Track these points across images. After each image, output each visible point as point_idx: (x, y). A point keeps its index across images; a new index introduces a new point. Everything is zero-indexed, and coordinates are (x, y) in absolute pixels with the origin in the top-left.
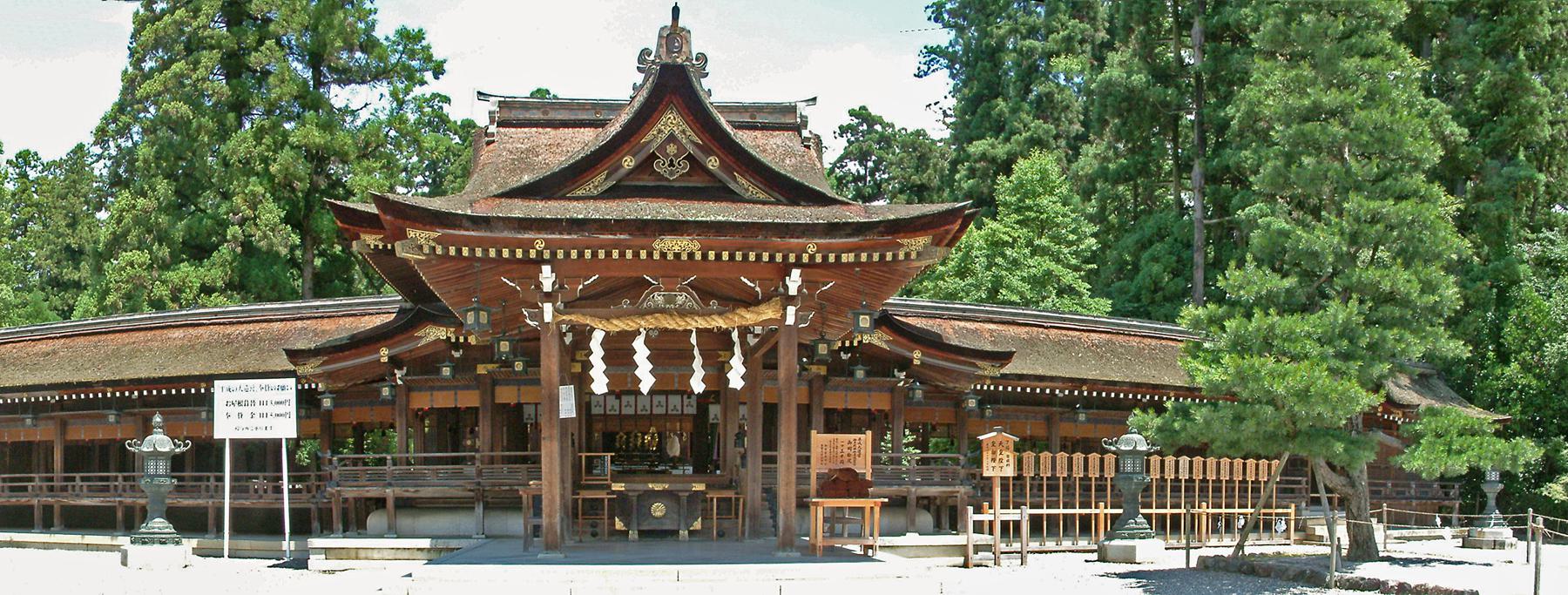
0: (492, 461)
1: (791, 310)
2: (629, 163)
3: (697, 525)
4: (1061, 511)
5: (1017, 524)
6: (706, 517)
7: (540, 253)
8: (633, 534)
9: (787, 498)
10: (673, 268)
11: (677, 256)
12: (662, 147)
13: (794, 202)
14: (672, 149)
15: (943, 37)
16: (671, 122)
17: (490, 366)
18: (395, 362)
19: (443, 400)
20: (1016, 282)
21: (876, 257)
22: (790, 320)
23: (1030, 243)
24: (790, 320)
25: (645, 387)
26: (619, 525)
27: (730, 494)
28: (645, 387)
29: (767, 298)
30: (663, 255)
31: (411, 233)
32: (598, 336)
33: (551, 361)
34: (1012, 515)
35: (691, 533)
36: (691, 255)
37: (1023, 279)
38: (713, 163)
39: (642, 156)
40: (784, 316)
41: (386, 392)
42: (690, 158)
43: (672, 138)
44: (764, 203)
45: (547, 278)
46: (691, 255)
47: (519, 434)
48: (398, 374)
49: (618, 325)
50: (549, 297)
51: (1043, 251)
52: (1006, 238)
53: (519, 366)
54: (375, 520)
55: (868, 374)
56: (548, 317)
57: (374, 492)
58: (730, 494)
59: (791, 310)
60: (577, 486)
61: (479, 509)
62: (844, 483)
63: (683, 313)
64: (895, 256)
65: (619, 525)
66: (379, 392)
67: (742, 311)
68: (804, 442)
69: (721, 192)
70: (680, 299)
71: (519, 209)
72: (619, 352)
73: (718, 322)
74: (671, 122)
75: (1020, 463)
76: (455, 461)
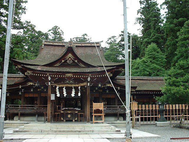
0: (40, 107)
1: (89, 83)
2: (63, 61)
3: (76, 119)
4: (154, 116)
5: (138, 119)
6: (78, 117)
7: (48, 76)
8: (64, 121)
9: (88, 114)
10: (69, 78)
11: (69, 76)
12: (68, 59)
13: (89, 67)
14: (70, 59)
15: (139, 16)
16: (70, 55)
17: (40, 90)
18: (22, 88)
19: (31, 95)
20: (148, 70)
21: (101, 76)
22: (89, 85)
23: (151, 61)
24: (89, 85)
25: (65, 96)
26: (62, 119)
27: (82, 113)
28: (65, 96)
29: (85, 82)
30: (67, 76)
31: (28, 71)
32: (58, 87)
33: (50, 91)
34: (137, 117)
35: (75, 121)
36: (71, 76)
37: (149, 69)
38: (76, 61)
39: (65, 60)
40: (88, 84)
41: (20, 93)
42: (73, 60)
43: (70, 57)
44: (84, 67)
45: (49, 78)
46: (71, 76)
47: (45, 101)
48: (23, 90)
49: (61, 86)
50: (49, 81)
51: (153, 63)
52: (146, 61)
53: (45, 90)
54: (15, 118)
55: (109, 91)
56: (49, 84)
57: (16, 112)
58: (82, 113)
59: (89, 83)
60: (55, 111)
61: (37, 116)
62: (98, 111)
63: (71, 84)
64: (104, 76)
65: (62, 119)
66: (19, 93)
67: (81, 84)
68: (91, 105)
69: (76, 65)
70: (71, 82)
71: (45, 69)
72: (61, 89)
73: (77, 85)
74: (70, 55)
75: (138, 106)
76: (33, 107)
